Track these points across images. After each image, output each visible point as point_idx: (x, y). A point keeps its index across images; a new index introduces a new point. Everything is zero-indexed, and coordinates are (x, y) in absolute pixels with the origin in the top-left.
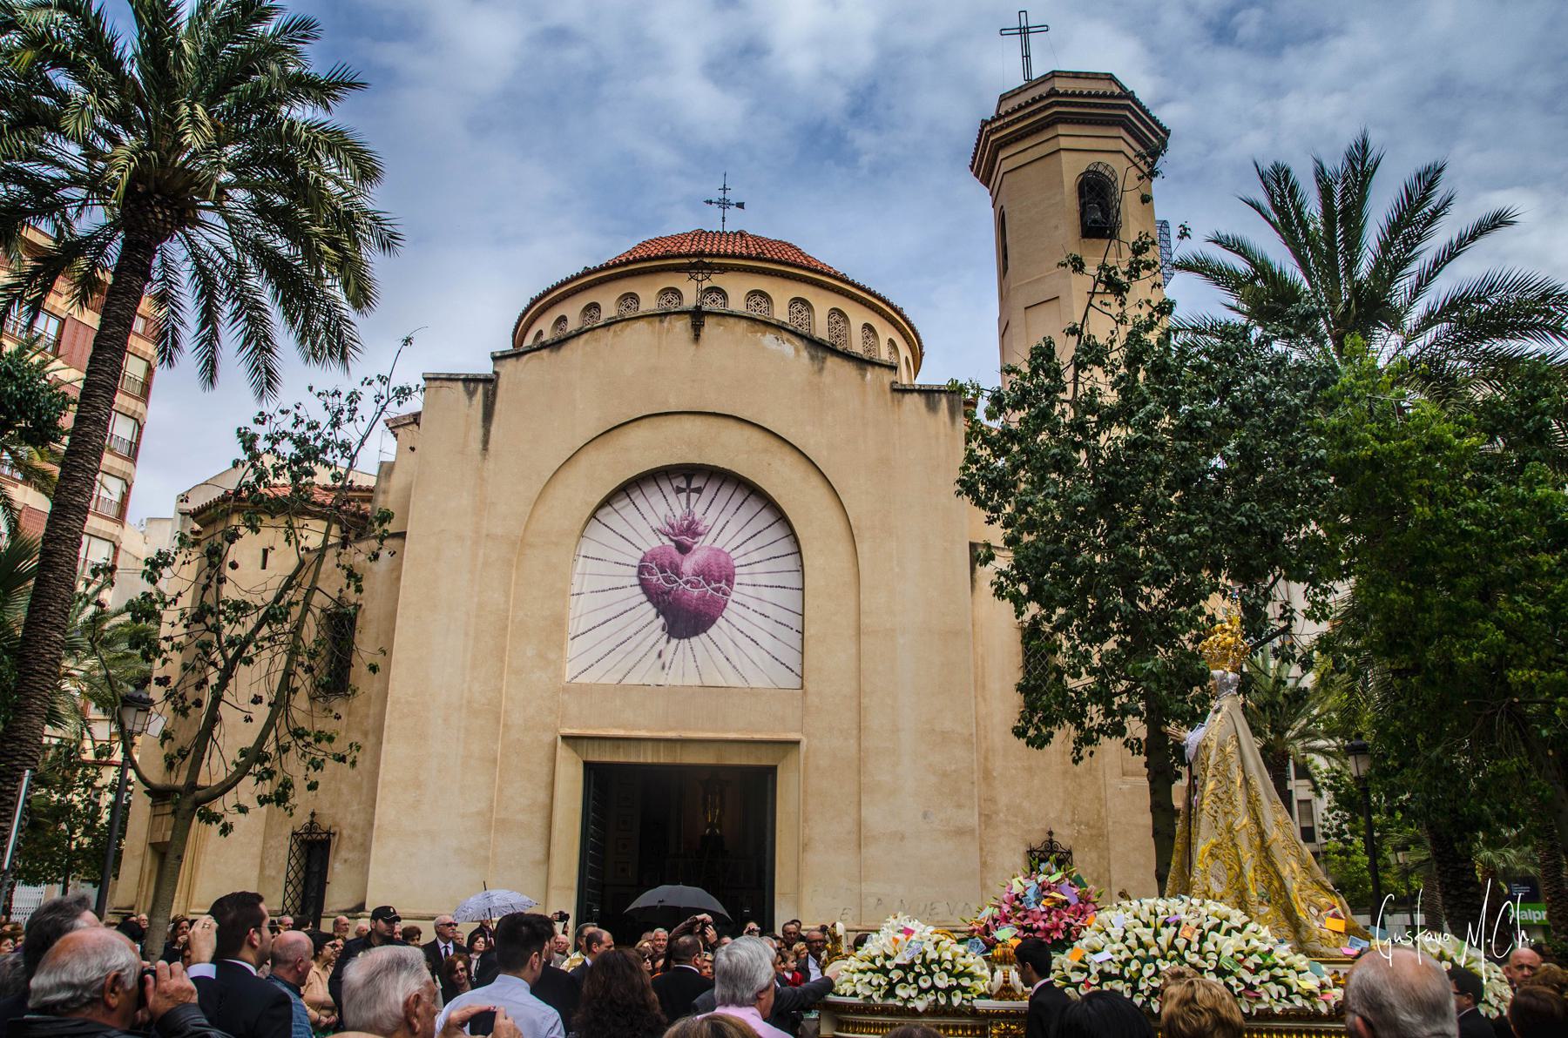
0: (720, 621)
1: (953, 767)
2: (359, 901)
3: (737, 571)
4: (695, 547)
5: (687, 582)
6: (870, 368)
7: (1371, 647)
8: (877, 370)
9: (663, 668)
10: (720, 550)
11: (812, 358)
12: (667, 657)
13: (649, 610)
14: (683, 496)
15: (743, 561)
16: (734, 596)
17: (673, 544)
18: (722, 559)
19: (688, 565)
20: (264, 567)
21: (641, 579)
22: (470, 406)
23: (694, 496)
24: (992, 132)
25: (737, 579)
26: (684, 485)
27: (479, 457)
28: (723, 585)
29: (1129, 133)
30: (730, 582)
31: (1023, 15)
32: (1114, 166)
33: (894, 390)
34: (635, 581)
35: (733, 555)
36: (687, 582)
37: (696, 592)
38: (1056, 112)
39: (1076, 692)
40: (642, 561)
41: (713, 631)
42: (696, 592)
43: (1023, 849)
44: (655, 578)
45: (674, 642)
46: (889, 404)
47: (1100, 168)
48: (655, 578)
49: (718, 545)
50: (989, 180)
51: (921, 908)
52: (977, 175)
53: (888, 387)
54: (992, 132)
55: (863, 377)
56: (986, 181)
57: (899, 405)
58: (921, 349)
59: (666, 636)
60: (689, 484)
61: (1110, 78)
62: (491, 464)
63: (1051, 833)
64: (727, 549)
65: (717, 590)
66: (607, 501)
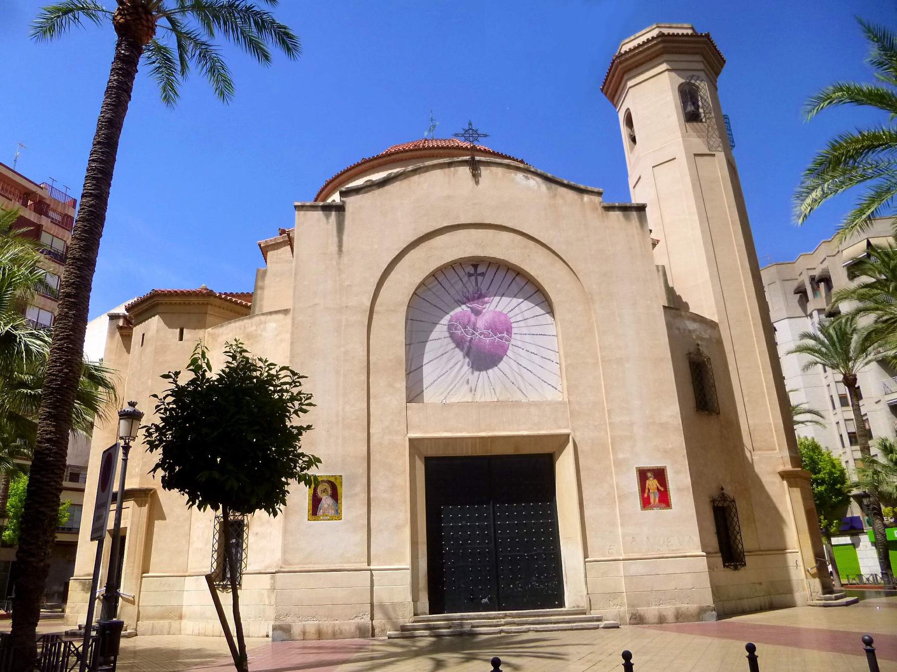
0: (505, 358)
1: (670, 446)
2: (778, 475)
3: (514, 325)
4: (484, 311)
5: (481, 334)
9: (471, 391)
10: (501, 313)
11: (548, 189)
12: (472, 384)
13: (459, 354)
14: (473, 278)
15: (519, 318)
16: (513, 342)
17: (469, 309)
18: (503, 318)
19: (481, 322)
20: (675, 158)
21: (450, 333)
22: (328, 223)
23: (480, 278)
24: (620, 63)
25: (514, 331)
26: (472, 271)
27: (336, 256)
28: (505, 335)
30: (509, 331)
34: (447, 334)
35: (510, 315)
36: (481, 334)
37: (488, 340)
38: (622, 69)
40: (450, 321)
41: (502, 365)
42: (488, 340)
43: (708, 500)
44: (459, 332)
45: (476, 373)
48: (459, 332)
49: (498, 309)
50: (614, 96)
51: (662, 542)
52: (606, 94)
54: (620, 63)
55: (582, 199)
59: (471, 370)
60: (476, 270)
62: (345, 259)
63: (722, 489)
64: (505, 312)
65: (501, 338)
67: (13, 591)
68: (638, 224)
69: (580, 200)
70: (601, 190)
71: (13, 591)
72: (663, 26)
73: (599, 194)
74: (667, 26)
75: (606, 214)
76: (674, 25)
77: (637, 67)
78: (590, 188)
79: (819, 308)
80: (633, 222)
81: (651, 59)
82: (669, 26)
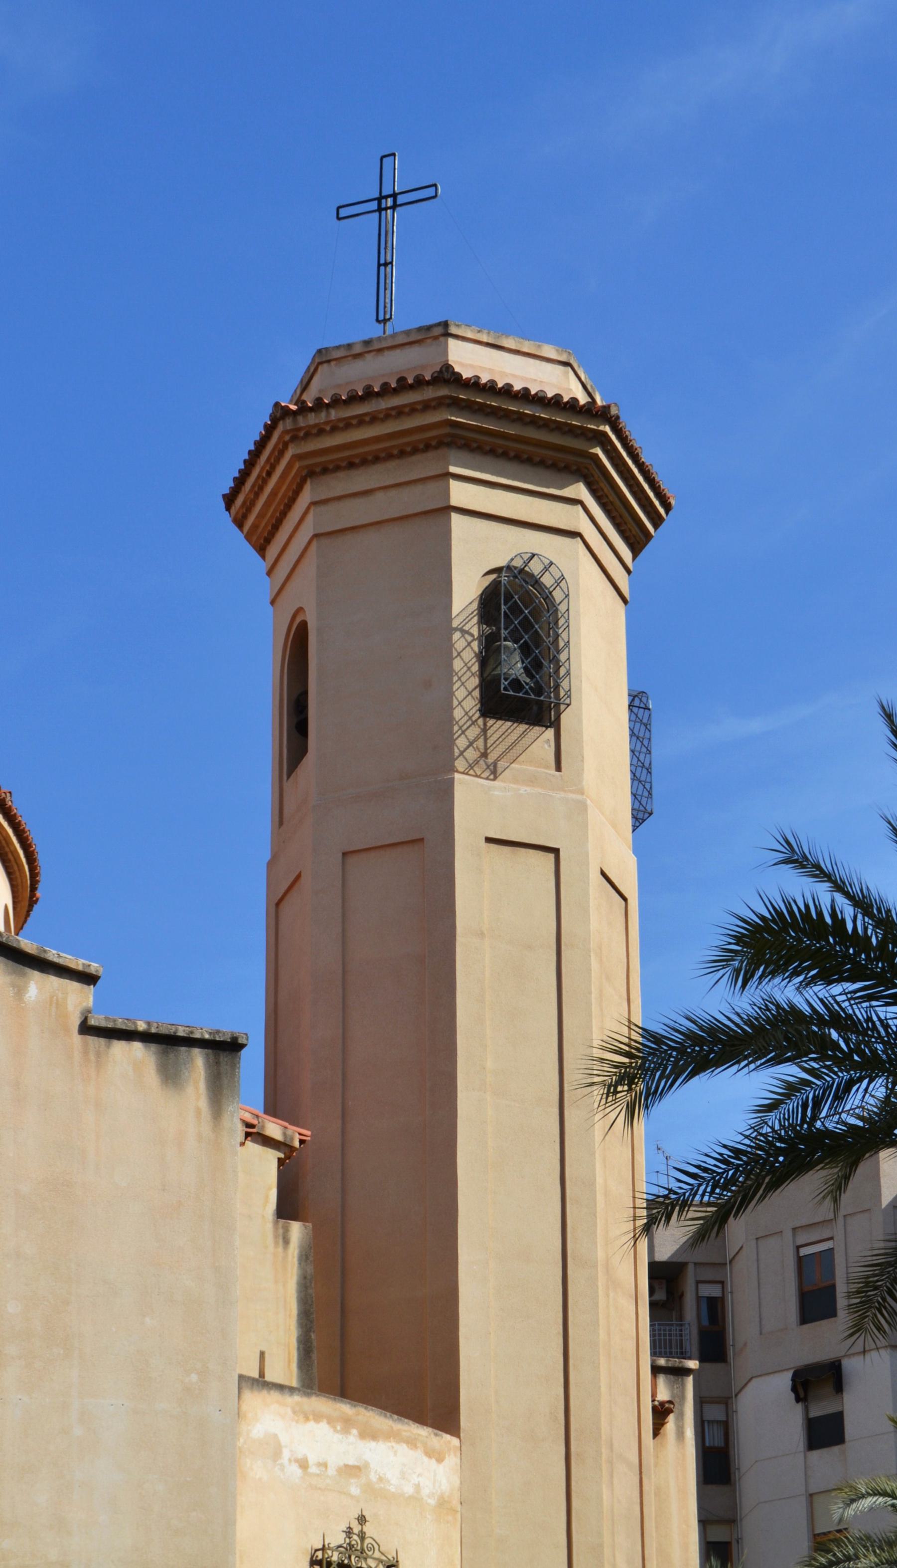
6: (36, 975)
7: (752, 1128)
8: (54, 981)
29: (594, 492)
31: (343, 212)
32: (563, 564)
33: (86, 1029)
39: (858, 1107)
46: (77, 1055)
47: (535, 567)
50: (268, 541)
52: (239, 523)
53: (76, 1022)
55: (20, 992)
56: (261, 550)
57: (99, 1065)
58: (33, 888)
61: (545, 392)
66: (755, 1206)
67: (517, 694)
68: (203, 1103)
69: (11, 992)
70: (94, 967)
71: (517, 694)
72: (469, 335)
73: (88, 979)
74: (484, 338)
75: (98, 1055)
76: (509, 343)
77: (351, 465)
78: (52, 955)
79: (696, 1261)
80: (190, 1090)
81: (402, 454)
82: (491, 341)
